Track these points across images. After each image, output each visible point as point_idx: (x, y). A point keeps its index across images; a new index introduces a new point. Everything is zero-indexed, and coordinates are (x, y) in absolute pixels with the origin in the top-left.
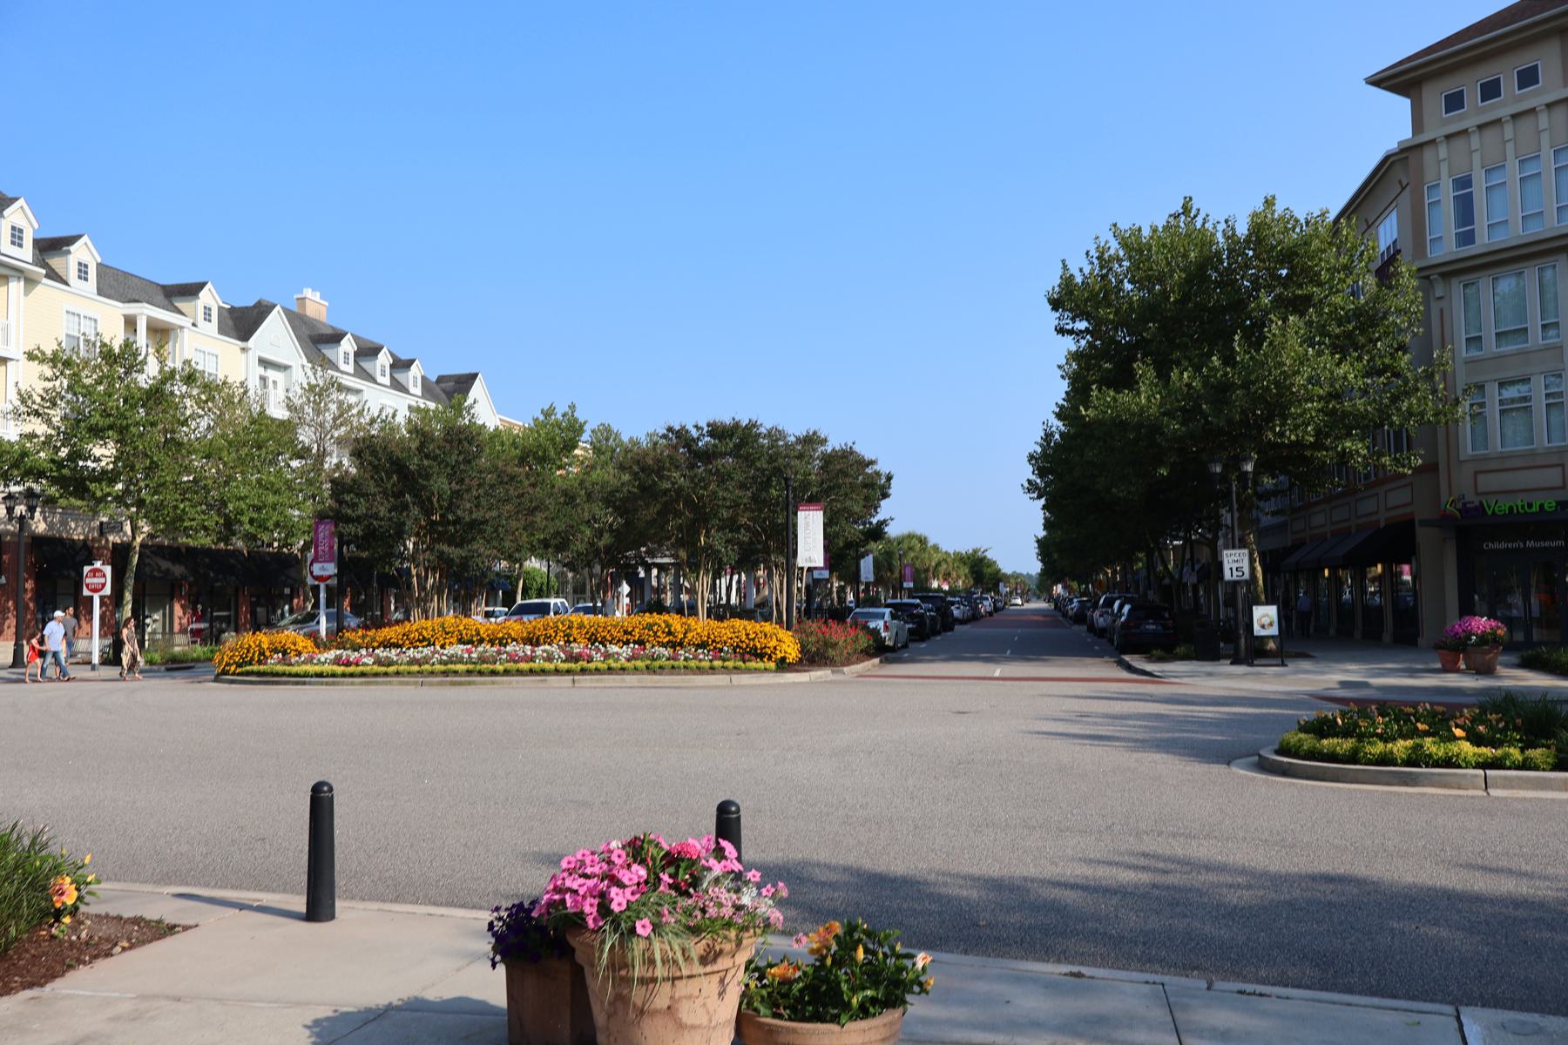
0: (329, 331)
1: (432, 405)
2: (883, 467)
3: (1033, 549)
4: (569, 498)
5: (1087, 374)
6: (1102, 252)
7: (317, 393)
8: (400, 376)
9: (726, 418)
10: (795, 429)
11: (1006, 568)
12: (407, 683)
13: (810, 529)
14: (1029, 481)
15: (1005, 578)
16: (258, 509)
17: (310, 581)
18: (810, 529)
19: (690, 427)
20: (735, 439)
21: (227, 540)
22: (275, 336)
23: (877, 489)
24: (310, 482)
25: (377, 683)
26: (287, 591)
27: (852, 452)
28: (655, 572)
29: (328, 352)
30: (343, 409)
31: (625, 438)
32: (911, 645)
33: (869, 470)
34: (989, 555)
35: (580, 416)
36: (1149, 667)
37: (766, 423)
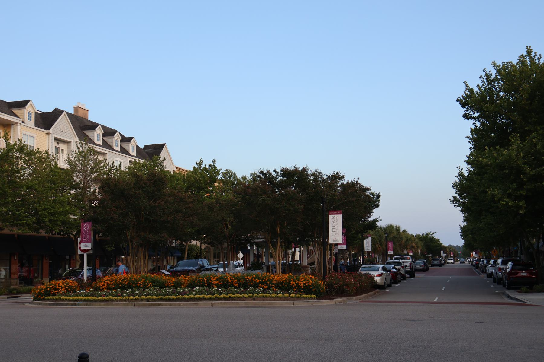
0: (90, 124)
1: (142, 161)
2: (375, 190)
3: (459, 232)
4: (210, 208)
5: (479, 139)
6: (488, 77)
7: (83, 156)
8: (125, 145)
9: (291, 167)
10: (327, 171)
11: (445, 242)
12: (128, 305)
13: (335, 225)
14: (454, 197)
15: (444, 248)
16: (53, 214)
17: (79, 252)
18: (335, 225)
19: (271, 171)
20: (296, 177)
21: (37, 230)
22: (63, 128)
23: (372, 202)
24: (79, 201)
25: (112, 305)
26: (68, 257)
27: (357, 184)
28: (255, 247)
29: (88, 133)
30: (97, 162)
31: (239, 176)
32: (393, 285)
33: (368, 193)
34: (436, 236)
35: (218, 166)
36: (519, 297)
37: (312, 168)
